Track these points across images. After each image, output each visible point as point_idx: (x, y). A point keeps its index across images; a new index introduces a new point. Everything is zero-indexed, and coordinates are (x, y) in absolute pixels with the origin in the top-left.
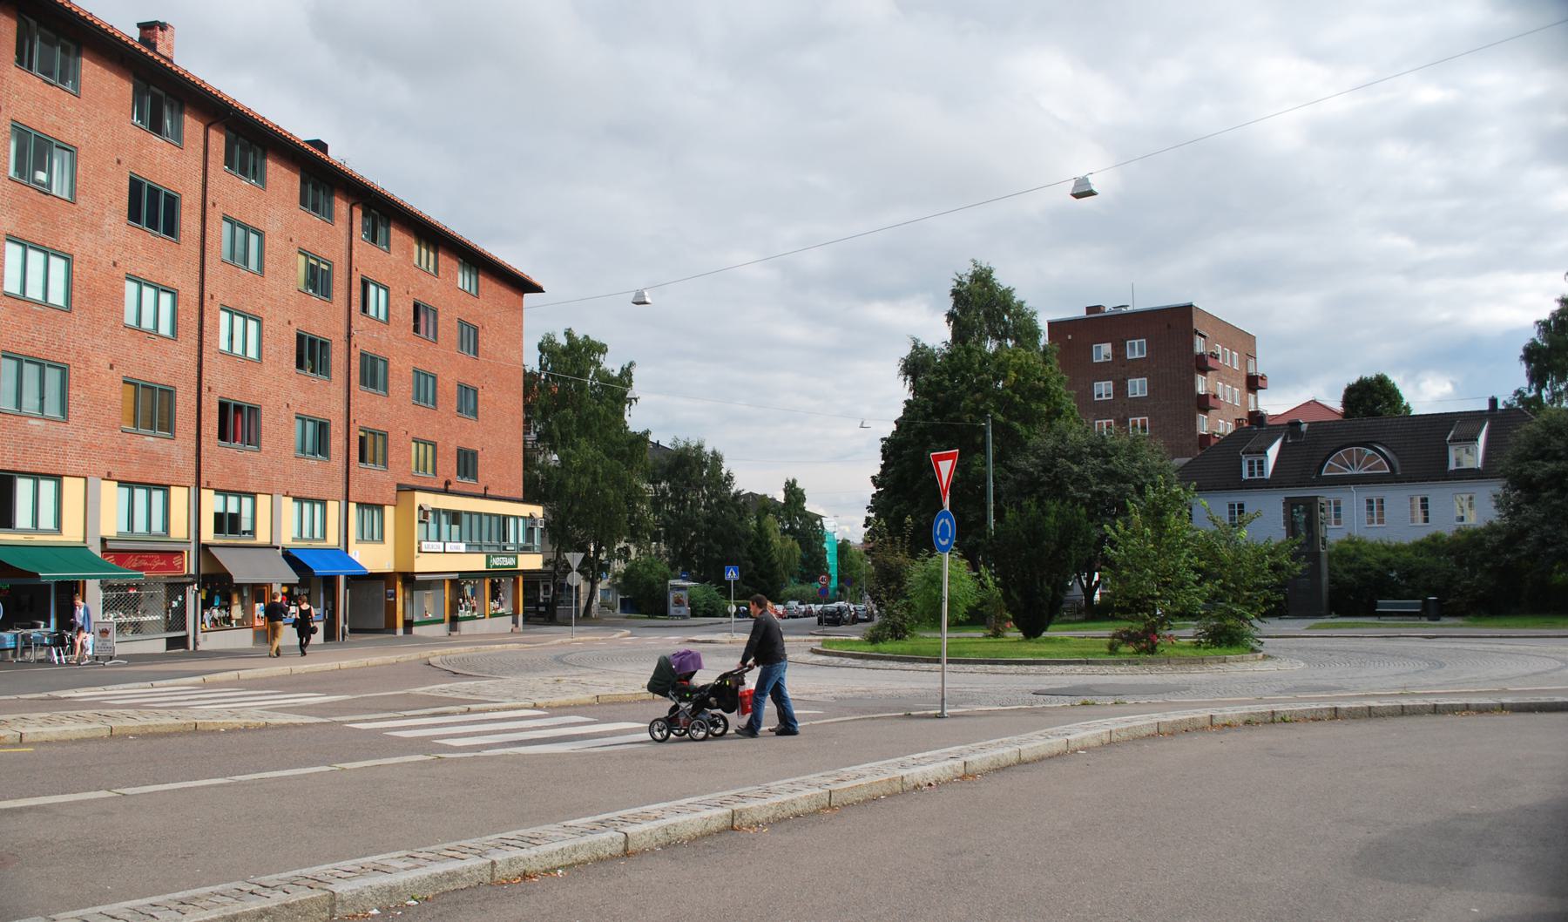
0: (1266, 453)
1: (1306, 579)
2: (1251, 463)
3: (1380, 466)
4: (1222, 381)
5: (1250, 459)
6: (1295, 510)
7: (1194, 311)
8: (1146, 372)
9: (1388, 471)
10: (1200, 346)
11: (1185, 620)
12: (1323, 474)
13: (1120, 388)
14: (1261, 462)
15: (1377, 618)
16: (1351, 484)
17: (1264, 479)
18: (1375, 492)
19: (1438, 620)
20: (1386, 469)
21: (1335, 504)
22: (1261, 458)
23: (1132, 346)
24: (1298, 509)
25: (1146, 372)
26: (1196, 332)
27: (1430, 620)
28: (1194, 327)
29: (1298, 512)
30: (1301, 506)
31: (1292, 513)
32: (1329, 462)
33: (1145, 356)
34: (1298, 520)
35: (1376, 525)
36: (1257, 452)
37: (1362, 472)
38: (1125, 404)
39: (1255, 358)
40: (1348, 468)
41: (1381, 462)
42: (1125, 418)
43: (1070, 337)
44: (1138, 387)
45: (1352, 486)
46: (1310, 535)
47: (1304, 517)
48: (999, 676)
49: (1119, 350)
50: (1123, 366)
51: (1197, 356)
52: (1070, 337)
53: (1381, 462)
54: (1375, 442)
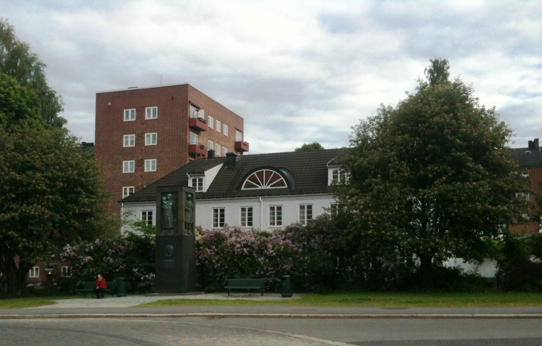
0: (204, 173)
1: (171, 260)
2: (194, 181)
3: (281, 183)
4: (212, 140)
5: (194, 178)
6: (164, 198)
7: (189, 89)
8: (156, 129)
9: (286, 187)
10: (193, 113)
11: (27, 307)
12: (243, 189)
13: (140, 139)
14: (201, 180)
15: (227, 295)
16: (260, 196)
17: (202, 193)
18: (276, 202)
19: (290, 296)
20: (285, 185)
21: (248, 211)
22: (201, 177)
23: (149, 111)
24: (167, 197)
25: (156, 129)
26: (190, 102)
27: (284, 296)
28: (189, 99)
29: (167, 200)
30: (170, 195)
31: (162, 200)
32: (247, 180)
33: (156, 118)
34: (166, 207)
35: (276, 226)
36: (198, 173)
37: (269, 187)
38: (142, 150)
39: (242, 132)
40: (259, 184)
41: (282, 180)
42: (142, 159)
43: (109, 104)
44: (150, 140)
45: (260, 198)
46: (175, 220)
47: (171, 204)
48: (417, 320)
49: (140, 114)
50: (143, 124)
51: (190, 119)
52: (109, 104)
53: (282, 180)
54: (282, 168)
